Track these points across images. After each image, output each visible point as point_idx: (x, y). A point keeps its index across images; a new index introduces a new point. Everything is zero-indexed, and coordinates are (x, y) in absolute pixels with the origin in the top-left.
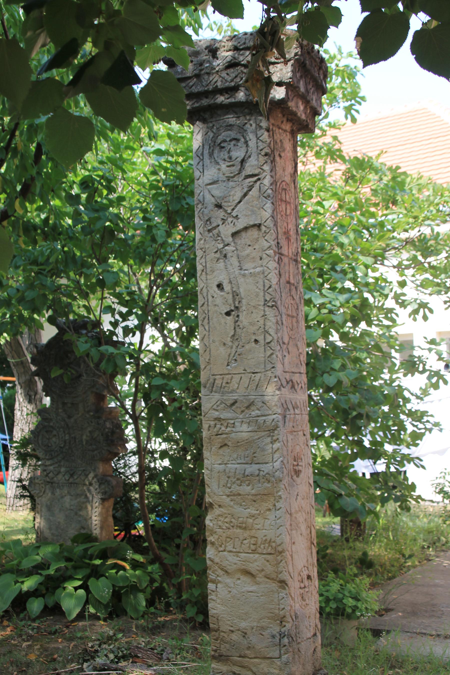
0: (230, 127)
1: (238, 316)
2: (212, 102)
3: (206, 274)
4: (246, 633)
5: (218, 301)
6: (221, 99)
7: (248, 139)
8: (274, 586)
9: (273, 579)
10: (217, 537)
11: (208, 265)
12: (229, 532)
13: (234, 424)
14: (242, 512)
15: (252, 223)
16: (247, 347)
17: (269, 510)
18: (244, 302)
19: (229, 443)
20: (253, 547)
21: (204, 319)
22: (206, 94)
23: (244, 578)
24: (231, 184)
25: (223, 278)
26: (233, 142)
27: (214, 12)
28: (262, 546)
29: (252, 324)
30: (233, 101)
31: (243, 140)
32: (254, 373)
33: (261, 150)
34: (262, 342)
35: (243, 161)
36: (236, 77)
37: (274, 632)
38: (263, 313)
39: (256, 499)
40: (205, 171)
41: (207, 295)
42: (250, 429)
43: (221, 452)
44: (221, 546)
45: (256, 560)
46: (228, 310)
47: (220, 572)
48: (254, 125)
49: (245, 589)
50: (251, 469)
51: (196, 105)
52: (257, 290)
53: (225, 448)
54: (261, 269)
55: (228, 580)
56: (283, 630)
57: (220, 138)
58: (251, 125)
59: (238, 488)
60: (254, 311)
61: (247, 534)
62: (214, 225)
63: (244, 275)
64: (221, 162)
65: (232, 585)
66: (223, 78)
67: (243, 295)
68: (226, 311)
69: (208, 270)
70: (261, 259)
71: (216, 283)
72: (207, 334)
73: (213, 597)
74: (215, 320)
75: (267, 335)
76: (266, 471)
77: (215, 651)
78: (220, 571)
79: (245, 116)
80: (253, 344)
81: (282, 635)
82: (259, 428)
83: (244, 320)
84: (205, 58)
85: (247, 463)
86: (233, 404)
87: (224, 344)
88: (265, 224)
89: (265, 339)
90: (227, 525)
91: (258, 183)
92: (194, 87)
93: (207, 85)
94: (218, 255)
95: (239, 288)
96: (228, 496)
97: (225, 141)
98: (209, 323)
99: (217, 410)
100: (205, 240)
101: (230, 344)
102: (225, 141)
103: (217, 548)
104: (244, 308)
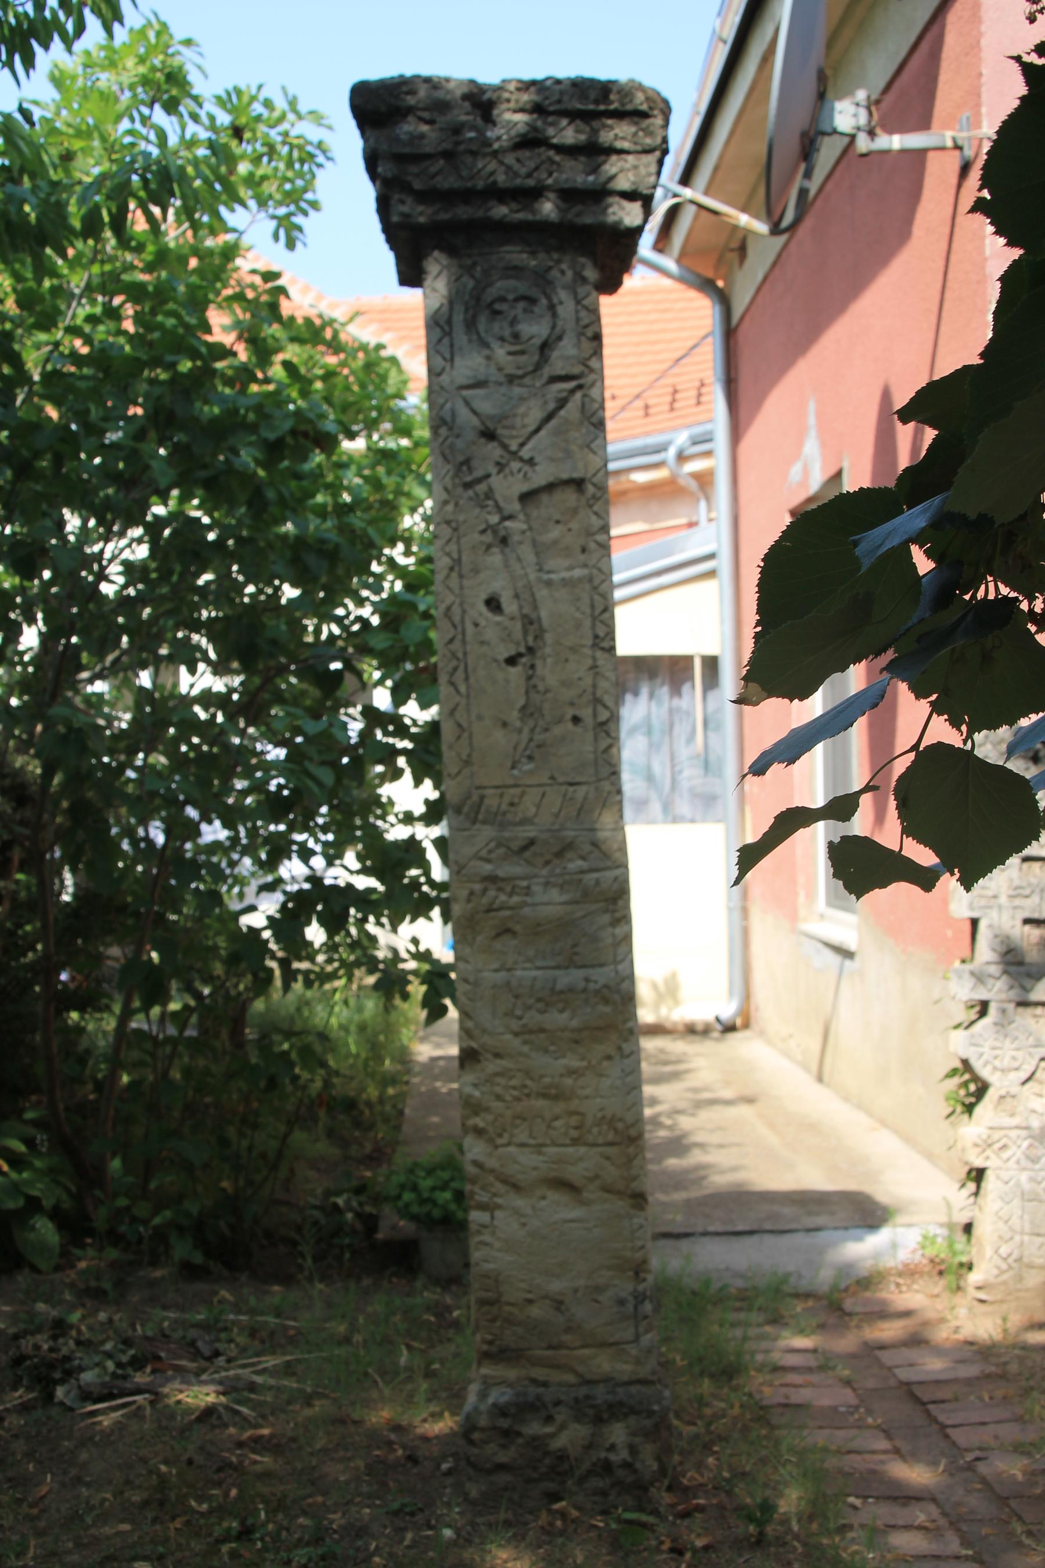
0: (515, 271)
1: (533, 667)
2: (480, 214)
3: (461, 576)
4: (561, 1302)
6: (500, 211)
7: (555, 301)
8: (620, 1205)
10: (490, 1118)
11: (464, 558)
13: (528, 887)
14: (552, 1066)
15: (565, 476)
16: (557, 730)
17: (609, 1058)
18: (549, 637)
19: (517, 928)
20: (574, 1134)
21: (455, 669)
22: (467, 196)
24: (517, 391)
25: (499, 585)
26: (521, 305)
28: (595, 1130)
29: (566, 684)
30: (530, 217)
31: (544, 301)
32: (572, 784)
33: (586, 326)
34: (589, 721)
35: (545, 347)
36: (537, 168)
37: (623, 1295)
38: (590, 662)
39: (577, 1039)
41: (463, 621)
43: (498, 945)
44: (500, 1136)
45: (581, 1159)
46: (513, 652)
47: (499, 1187)
48: (569, 274)
50: (572, 977)
51: (444, 216)
52: (578, 615)
53: (506, 938)
54: (585, 572)
56: (641, 1287)
57: (492, 292)
58: (563, 272)
59: (539, 1017)
61: (559, 1108)
62: (479, 473)
63: (549, 583)
64: (495, 345)
65: (529, 1211)
66: (509, 168)
67: (546, 622)
68: (506, 655)
69: (466, 568)
70: (584, 550)
71: (484, 596)
72: (463, 702)
73: (486, 1238)
75: (600, 708)
76: (602, 981)
77: (490, 1343)
79: (548, 252)
80: (570, 726)
81: (640, 1298)
82: (586, 896)
83: (548, 673)
84: (463, 118)
86: (525, 848)
87: (505, 724)
88: (595, 480)
89: (595, 715)
90: (515, 1093)
91: (578, 395)
92: (439, 178)
93: (472, 178)
94: (488, 538)
95: (535, 607)
96: (516, 1034)
97: (502, 299)
98: (467, 679)
99: (488, 861)
100: (456, 504)
101: (518, 724)
102: (502, 299)
103: (491, 1141)
104: (548, 650)
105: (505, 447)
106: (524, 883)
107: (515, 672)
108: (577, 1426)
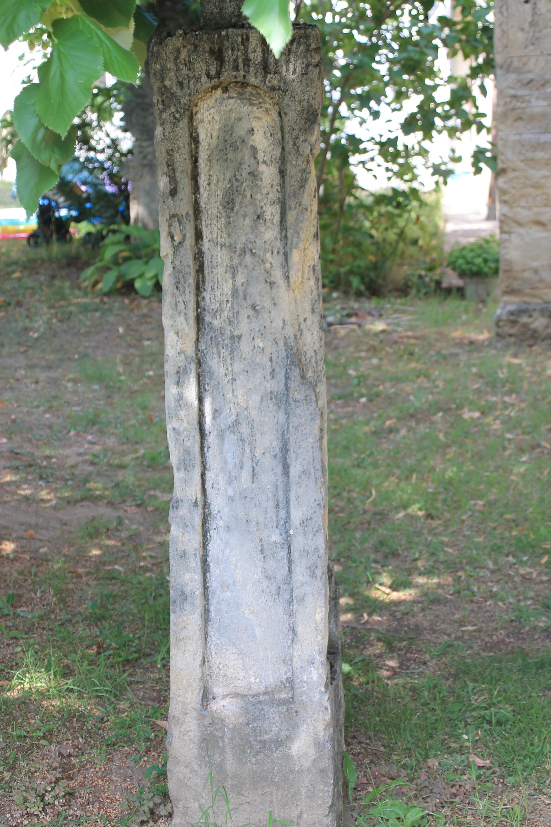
23: (536, 228)
27: (34, 68)
47: (513, 224)
55: (521, 231)
61: (539, 192)
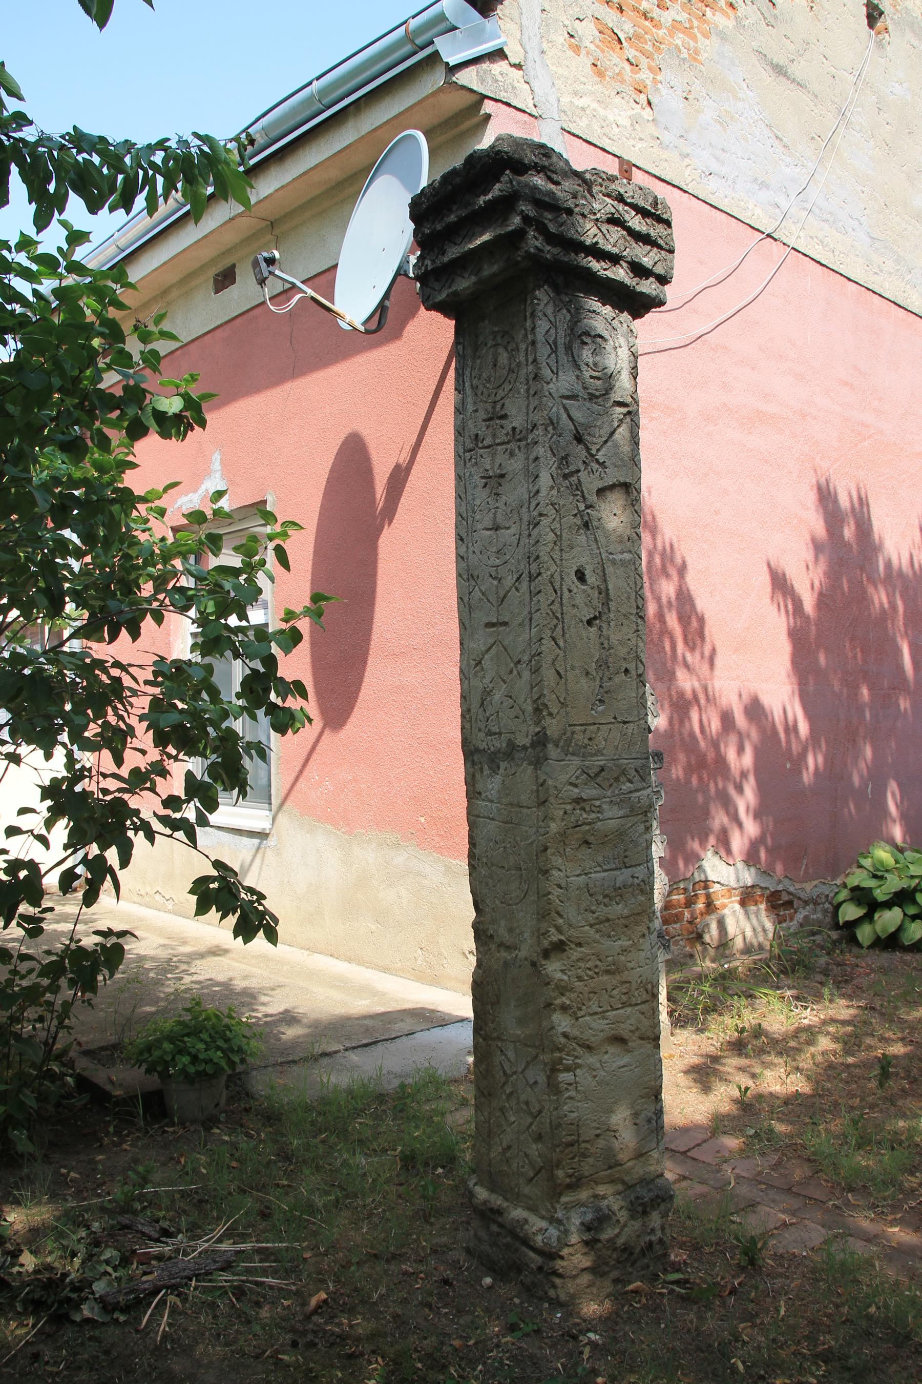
5: (579, 600)
9: (648, 1038)
12: (592, 984)
34: (633, 673)
37: (650, 1114)
40: (560, 373)
41: (561, 589)
42: (621, 813)
44: (580, 1009)
49: (615, 1065)
50: (623, 876)
55: (591, 1060)
60: (625, 622)
62: (572, 468)
63: (614, 562)
69: (565, 544)
74: (573, 630)
78: (578, 1049)
85: (616, 869)
87: (587, 673)
99: (576, 786)
105: (588, 450)
106: (598, 803)
107: (593, 630)
108: (633, 1222)
